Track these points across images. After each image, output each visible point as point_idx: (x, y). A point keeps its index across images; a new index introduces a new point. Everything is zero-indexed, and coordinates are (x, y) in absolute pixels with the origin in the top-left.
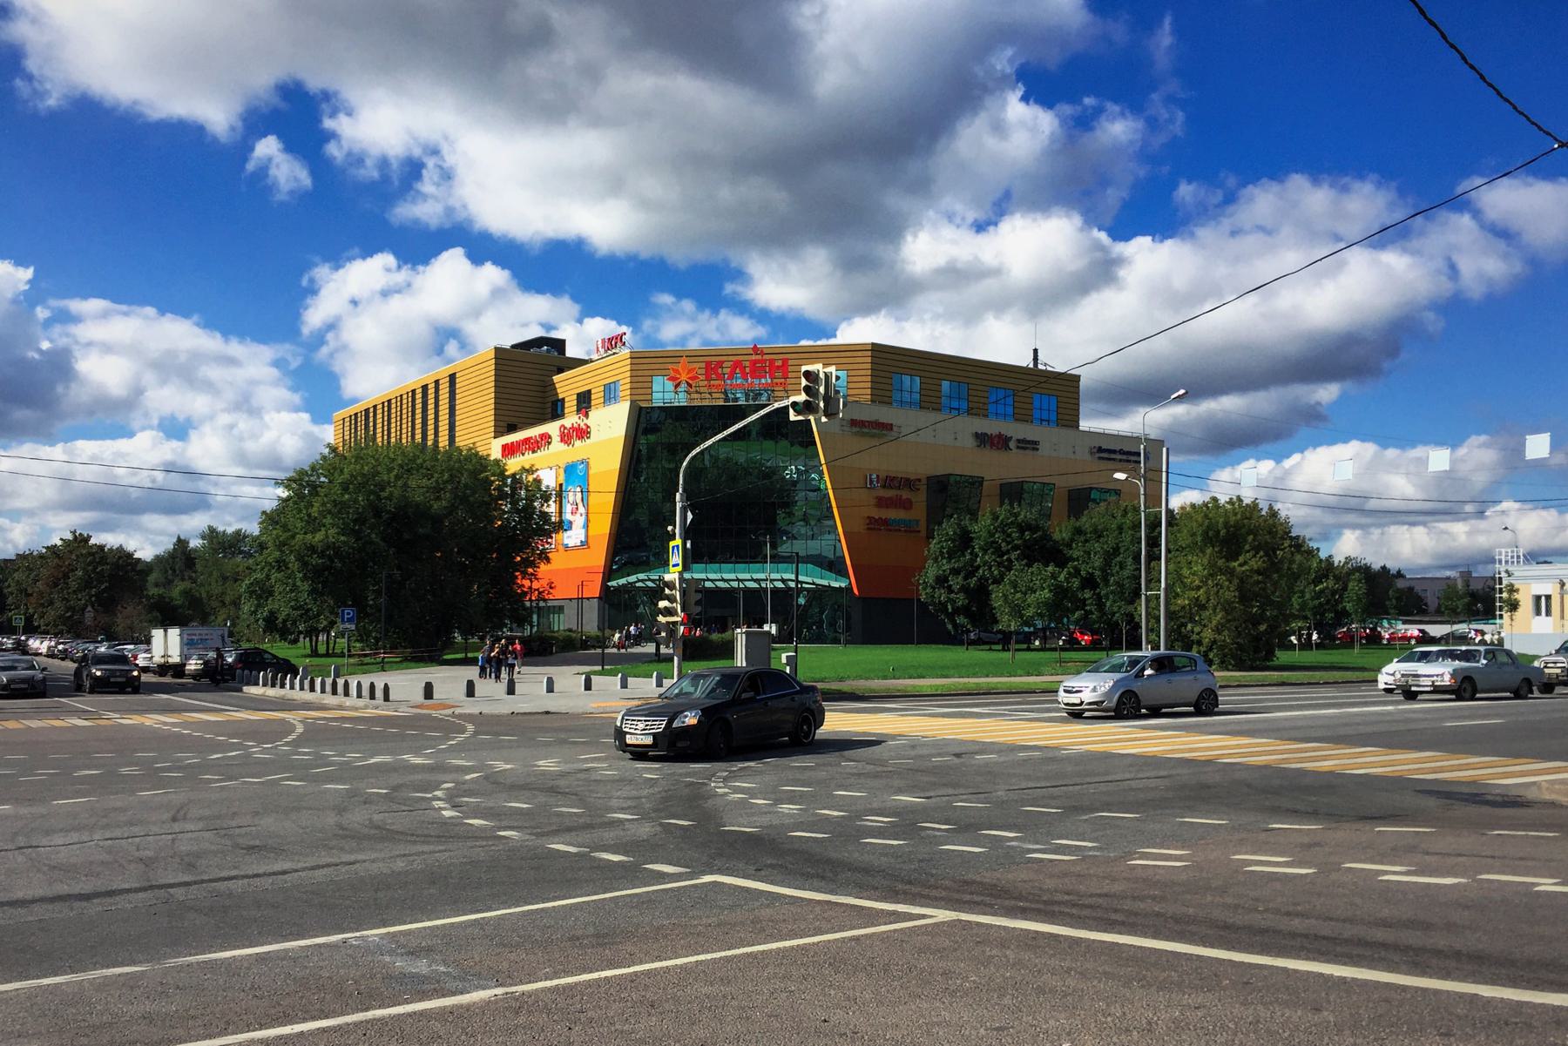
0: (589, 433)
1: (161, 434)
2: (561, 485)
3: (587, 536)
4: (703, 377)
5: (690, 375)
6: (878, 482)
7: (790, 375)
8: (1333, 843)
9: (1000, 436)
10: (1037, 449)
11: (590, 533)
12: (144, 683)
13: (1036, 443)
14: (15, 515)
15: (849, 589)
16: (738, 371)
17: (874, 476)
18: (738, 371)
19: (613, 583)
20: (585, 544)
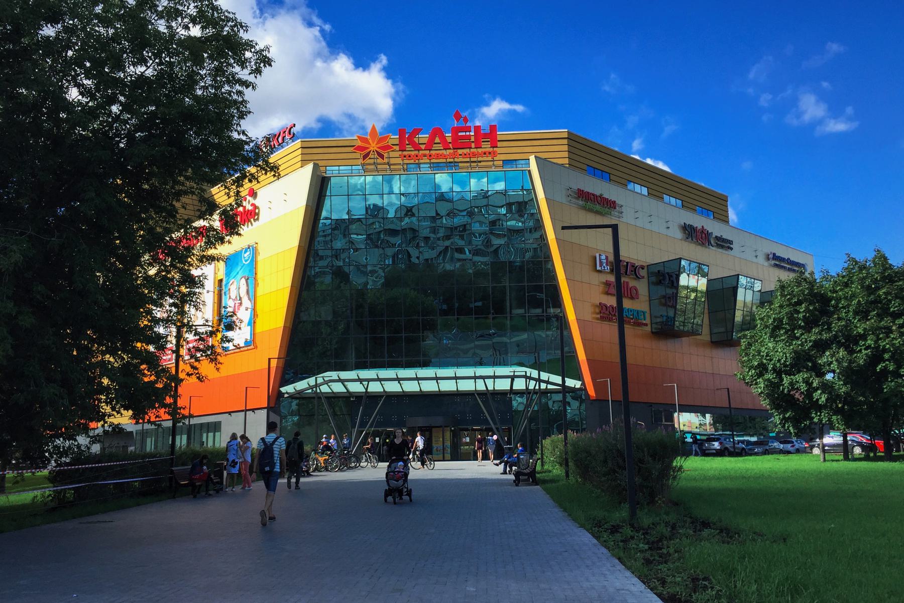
0: (258, 214)
1: (545, 492)
2: (221, 281)
3: (253, 334)
4: (397, 148)
5: (379, 145)
6: (607, 265)
7: (499, 144)
8: (701, 520)
9: (703, 230)
10: (732, 249)
11: (258, 329)
12: (412, 480)
13: (731, 242)
14: (577, 481)
15: (583, 389)
16: (437, 140)
17: (603, 257)
18: (437, 140)
19: (288, 389)
20: (251, 343)
